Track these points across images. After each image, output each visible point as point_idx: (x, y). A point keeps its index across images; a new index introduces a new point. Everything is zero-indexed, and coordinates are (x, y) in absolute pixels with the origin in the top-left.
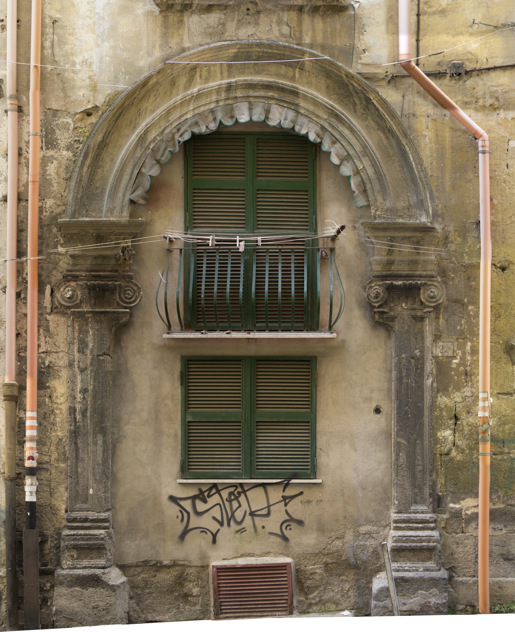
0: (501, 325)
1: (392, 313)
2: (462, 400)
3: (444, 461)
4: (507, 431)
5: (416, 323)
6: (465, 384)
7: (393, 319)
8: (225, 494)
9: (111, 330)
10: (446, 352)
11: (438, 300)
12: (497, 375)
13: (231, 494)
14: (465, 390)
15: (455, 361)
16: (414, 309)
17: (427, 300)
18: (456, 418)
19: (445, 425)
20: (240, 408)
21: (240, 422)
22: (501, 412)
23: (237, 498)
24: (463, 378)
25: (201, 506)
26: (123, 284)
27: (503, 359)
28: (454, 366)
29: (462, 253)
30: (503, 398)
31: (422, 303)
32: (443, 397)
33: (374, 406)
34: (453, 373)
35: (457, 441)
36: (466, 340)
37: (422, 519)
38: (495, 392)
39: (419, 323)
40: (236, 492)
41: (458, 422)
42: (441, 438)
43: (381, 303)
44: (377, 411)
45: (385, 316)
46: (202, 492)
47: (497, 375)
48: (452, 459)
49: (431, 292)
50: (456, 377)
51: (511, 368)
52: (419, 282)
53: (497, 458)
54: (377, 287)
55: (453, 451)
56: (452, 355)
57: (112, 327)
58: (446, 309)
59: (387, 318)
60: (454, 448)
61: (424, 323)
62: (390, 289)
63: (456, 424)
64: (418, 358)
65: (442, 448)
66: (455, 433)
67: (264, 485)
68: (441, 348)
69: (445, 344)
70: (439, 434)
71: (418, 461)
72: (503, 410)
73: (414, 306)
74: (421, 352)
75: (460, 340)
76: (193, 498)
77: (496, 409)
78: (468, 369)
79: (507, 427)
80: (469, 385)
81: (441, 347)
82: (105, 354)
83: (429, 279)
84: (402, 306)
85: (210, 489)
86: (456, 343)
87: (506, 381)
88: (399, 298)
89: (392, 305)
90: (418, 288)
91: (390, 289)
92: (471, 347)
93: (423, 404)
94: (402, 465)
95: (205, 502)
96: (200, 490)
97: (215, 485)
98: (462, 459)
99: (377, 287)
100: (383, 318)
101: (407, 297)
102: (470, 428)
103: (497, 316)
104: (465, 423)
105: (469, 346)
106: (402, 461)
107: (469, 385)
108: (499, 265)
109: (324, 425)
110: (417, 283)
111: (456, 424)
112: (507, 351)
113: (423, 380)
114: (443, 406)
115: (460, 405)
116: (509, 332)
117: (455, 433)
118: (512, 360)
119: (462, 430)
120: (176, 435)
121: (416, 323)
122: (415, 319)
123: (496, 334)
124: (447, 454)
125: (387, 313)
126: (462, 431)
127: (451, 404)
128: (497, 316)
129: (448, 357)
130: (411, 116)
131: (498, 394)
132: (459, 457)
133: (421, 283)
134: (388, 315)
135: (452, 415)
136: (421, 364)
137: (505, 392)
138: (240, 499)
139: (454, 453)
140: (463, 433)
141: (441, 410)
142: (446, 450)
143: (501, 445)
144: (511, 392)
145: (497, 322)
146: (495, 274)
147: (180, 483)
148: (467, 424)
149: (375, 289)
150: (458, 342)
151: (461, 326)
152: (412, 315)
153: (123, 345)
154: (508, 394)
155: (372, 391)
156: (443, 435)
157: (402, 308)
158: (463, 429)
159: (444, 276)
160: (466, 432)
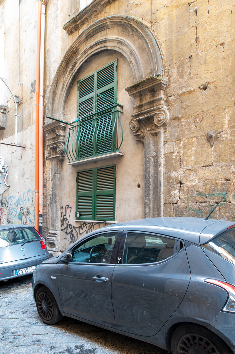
0: (204, 124)
1: (142, 135)
2: (183, 173)
3: (175, 207)
4: (208, 189)
5: (154, 137)
6: (180, 167)
7: (143, 137)
8: (88, 226)
9: (58, 163)
10: (170, 150)
11: (163, 121)
12: (202, 155)
13: (89, 226)
14: (180, 170)
15: (174, 155)
16: (152, 130)
17: (157, 123)
18: (181, 183)
19: (175, 187)
20: (92, 190)
21: (92, 196)
22: (204, 177)
23: (91, 228)
24: (179, 163)
25: (81, 231)
26: (58, 145)
27: (205, 145)
28: (174, 157)
29: (182, 87)
30: (205, 169)
31: (156, 125)
32: (174, 172)
33: (137, 184)
34: (173, 162)
35: (181, 196)
36: (180, 140)
37: (156, 243)
38: (201, 166)
39: (155, 137)
40: (91, 226)
41: (182, 185)
42: (173, 195)
43: (136, 130)
44: (139, 186)
45: (139, 137)
46: (81, 225)
47: (202, 155)
48: (179, 206)
49: (159, 118)
50: (175, 164)
51: (210, 150)
52: (152, 114)
53: (202, 205)
54: (134, 122)
55: (179, 202)
56: (172, 151)
57: (58, 162)
58: (170, 125)
59: (141, 137)
60: (179, 200)
61: (158, 136)
62: (139, 121)
63: (180, 186)
64: (155, 157)
65: (174, 200)
66: (180, 191)
67: (99, 223)
68: (167, 149)
69: (169, 145)
70: (172, 193)
71: (156, 212)
72: (205, 176)
73: (152, 128)
74: (156, 153)
75: (177, 142)
76: (79, 227)
77: (202, 176)
78: (182, 157)
79: (208, 186)
80: (182, 167)
81: (167, 147)
82: (56, 173)
83: (158, 110)
84: (147, 129)
85: (84, 224)
86: (175, 143)
87: (208, 158)
88: (145, 125)
89: (142, 130)
90: (152, 117)
91: (139, 121)
92: (183, 144)
93: (158, 182)
94: (147, 214)
95: (82, 229)
96: (81, 224)
97: (85, 223)
98: (183, 206)
99: (134, 122)
100: (139, 138)
101: (149, 124)
102: (187, 188)
103: (201, 119)
104: (185, 186)
105: (182, 144)
106: (147, 212)
107: (182, 167)
108: (202, 87)
109: (117, 196)
110: (151, 115)
111: (180, 186)
112: (208, 140)
113: (158, 168)
114: (174, 177)
115: (182, 175)
116: (209, 127)
117: (180, 191)
118: (211, 145)
119: (183, 190)
120: (75, 202)
121: (154, 137)
122: (153, 135)
123: (201, 131)
124: (176, 203)
125: (140, 135)
126: (183, 190)
127: (178, 175)
128: (201, 119)
129: (170, 153)
130: (156, 12)
131: (203, 167)
132: (182, 205)
133: (153, 114)
134: (141, 136)
135: (178, 182)
136: (156, 160)
137: (207, 165)
138: (92, 229)
139: (179, 203)
140: (184, 191)
141: (173, 179)
142: (175, 201)
143: (205, 198)
144: (210, 164)
145: (202, 123)
146: (200, 93)
147: (76, 221)
148: (186, 186)
149: (134, 123)
150: (176, 143)
151: (178, 133)
152: (151, 133)
153: (63, 168)
154: (209, 166)
155: (136, 177)
156: (174, 193)
157: (147, 131)
158: (184, 189)
159: (169, 106)
160: (186, 191)
